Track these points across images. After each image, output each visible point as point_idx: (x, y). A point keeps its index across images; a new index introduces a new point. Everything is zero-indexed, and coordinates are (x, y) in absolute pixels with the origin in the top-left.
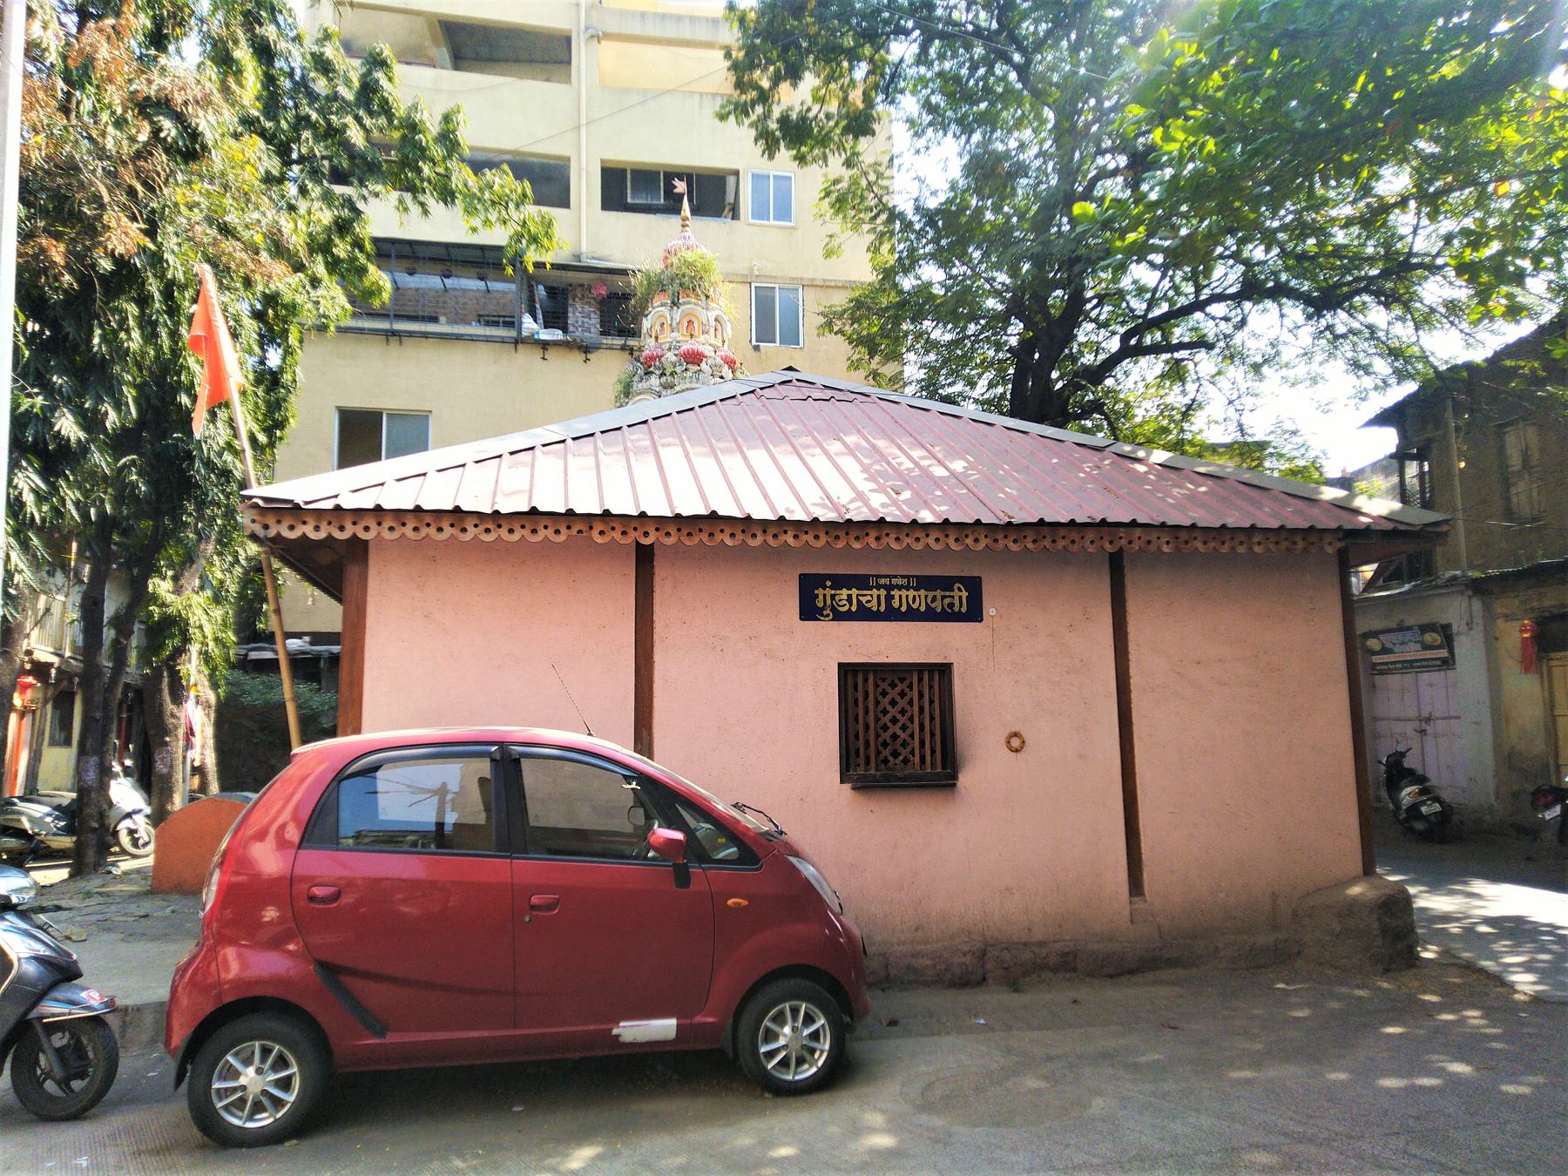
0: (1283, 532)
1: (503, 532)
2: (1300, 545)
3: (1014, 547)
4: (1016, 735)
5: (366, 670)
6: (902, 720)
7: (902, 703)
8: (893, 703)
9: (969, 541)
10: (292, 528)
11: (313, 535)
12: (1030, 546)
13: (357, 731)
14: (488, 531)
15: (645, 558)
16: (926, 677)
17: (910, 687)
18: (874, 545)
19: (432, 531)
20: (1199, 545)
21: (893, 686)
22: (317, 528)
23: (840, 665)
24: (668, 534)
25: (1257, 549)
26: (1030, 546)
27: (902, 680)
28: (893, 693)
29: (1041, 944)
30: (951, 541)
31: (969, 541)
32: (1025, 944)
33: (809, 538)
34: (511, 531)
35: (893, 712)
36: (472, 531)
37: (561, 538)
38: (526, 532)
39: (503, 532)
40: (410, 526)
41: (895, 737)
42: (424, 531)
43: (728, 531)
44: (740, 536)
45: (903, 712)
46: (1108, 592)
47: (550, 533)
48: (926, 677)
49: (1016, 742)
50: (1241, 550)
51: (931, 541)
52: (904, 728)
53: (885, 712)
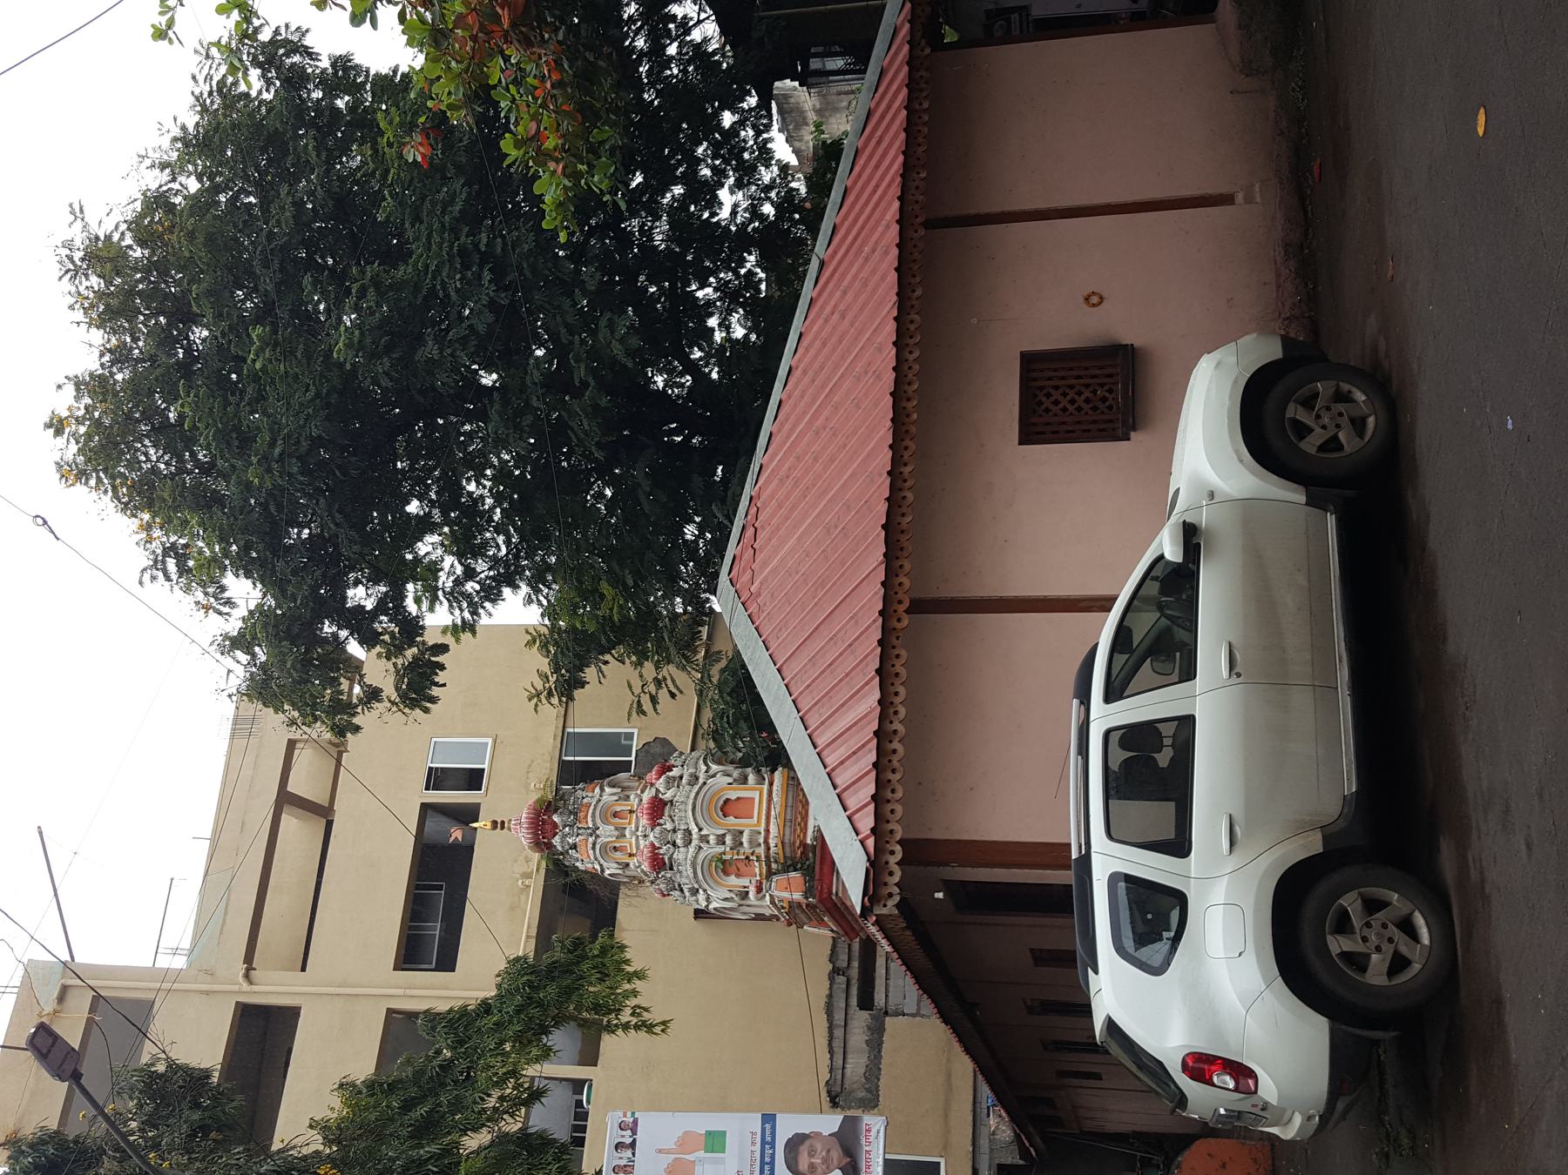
0: (912, 84)
1: (898, 700)
2: (922, 73)
3: (919, 292)
4: (1087, 299)
5: (1022, 840)
6: (1071, 395)
7: (1056, 395)
8: (1056, 403)
9: (912, 327)
10: (891, 874)
11: (899, 856)
12: (918, 279)
13: (1069, 845)
14: (896, 713)
15: (920, 606)
16: (1034, 375)
17: (1041, 388)
18: (898, 776)
19: (895, 759)
20: (921, 149)
21: (1041, 403)
22: (892, 853)
23: (1020, 443)
24: (892, 811)
25: (926, 105)
26: (918, 279)
27: (1036, 396)
28: (1047, 403)
29: (1278, 275)
30: (911, 341)
31: (912, 327)
32: (1279, 287)
33: (906, 455)
34: (896, 694)
35: (1064, 402)
36: (897, 726)
37: (903, 653)
38: (897, 682)
39: (898, 700)
40: (891, 776)
41: (1087, 401)
42: (895, 763)
43: (899, 519)
44: (904, 510)
45: (1065, 395)
46: (976, 50)
47: (898, 663)
48: (1034, 375)
49: (1094, 300)
50: (926, 118)
51: (911, 357)
52: (1079, 393)
53: (1065, 409)
